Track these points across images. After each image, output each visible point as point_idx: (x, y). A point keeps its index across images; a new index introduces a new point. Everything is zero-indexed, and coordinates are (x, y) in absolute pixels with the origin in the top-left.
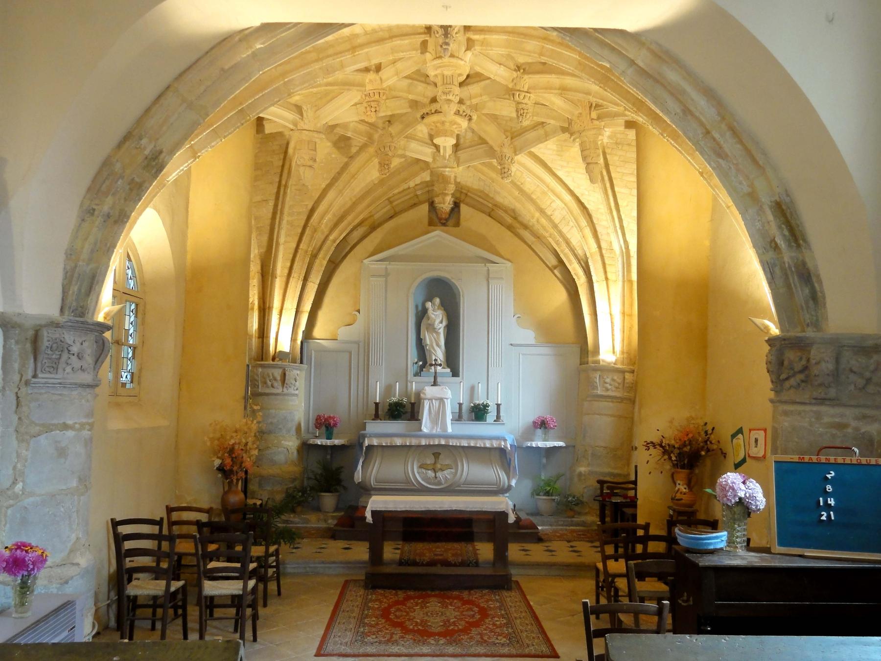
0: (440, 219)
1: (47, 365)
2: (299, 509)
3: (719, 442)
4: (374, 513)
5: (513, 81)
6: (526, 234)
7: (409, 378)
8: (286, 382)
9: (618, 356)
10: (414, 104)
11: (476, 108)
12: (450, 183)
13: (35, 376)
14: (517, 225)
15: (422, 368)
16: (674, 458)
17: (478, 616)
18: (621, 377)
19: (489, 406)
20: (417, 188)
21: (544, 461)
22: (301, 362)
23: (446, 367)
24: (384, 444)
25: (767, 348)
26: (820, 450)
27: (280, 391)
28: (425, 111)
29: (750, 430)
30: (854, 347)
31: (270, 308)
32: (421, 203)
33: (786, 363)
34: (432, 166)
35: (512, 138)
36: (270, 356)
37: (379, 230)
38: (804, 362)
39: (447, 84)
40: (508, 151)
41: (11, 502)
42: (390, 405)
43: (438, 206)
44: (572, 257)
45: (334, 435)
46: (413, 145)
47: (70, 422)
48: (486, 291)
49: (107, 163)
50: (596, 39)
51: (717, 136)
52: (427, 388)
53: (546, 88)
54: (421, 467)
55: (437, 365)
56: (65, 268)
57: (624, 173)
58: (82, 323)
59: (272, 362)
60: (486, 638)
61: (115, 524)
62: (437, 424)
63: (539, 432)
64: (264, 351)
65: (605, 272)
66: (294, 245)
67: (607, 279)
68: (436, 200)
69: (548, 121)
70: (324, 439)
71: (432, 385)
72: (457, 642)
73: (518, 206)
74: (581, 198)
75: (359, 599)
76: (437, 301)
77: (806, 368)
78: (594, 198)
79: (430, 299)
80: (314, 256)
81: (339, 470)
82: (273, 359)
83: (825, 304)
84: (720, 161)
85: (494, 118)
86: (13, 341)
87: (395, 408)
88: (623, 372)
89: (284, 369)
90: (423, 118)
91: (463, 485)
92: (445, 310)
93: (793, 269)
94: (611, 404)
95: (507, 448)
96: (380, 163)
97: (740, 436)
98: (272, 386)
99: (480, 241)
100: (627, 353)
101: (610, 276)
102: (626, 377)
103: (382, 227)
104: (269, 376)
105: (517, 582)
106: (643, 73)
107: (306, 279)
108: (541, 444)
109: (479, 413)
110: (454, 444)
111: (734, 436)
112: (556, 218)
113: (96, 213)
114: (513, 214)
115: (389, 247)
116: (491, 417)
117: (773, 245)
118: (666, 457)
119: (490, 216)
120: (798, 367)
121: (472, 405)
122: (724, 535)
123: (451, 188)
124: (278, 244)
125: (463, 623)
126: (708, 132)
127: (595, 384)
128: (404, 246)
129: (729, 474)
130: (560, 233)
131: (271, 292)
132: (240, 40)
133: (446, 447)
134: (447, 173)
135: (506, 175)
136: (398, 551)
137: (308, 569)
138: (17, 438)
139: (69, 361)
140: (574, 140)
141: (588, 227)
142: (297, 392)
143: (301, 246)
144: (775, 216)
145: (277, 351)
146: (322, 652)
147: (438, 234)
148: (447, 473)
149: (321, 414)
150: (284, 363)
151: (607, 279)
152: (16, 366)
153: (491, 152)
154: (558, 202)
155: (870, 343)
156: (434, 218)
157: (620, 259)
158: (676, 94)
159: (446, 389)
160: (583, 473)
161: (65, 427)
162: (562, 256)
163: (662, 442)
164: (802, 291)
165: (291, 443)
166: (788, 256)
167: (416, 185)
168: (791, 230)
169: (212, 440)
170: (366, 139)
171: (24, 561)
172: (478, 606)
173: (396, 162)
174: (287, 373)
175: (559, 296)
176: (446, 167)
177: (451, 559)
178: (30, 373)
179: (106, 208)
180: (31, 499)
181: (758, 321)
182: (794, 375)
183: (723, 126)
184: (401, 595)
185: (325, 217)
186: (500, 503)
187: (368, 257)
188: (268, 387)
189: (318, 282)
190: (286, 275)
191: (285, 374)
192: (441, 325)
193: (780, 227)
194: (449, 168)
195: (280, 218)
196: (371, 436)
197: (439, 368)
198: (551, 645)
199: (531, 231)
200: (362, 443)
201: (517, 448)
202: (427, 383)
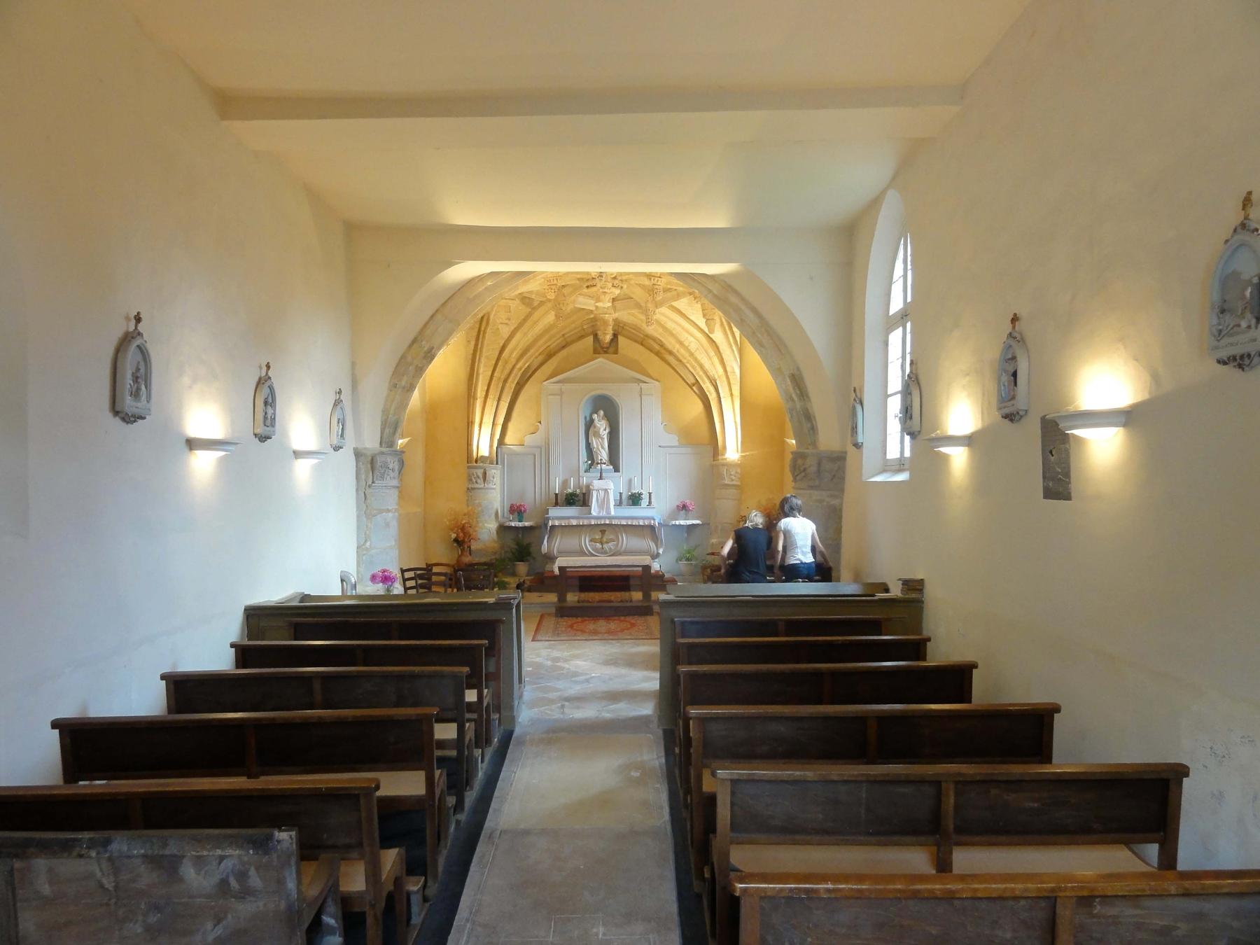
0: (602, 348)
4: (561, 568)
6: (671, 359)
7: (581, 474)
13: (373, 483)
14: (663, 351)
15: (591, 466)
17: (629, 626)
22: (497, 464)
27: (482, 486)
40: (650, 306)
41: (365, 552)
42: (567, 495)
45: (524, 520)
46: (581, 299)
47: (390, 508)
49: (403, 357)
58: (393, 451)
62: (603, 509)
66: (490, 373)
76: (602, 413)
77: (805, 470)
80: (505, 381)
81: (529, 545)
82: (476, 462)
90: (588, 287)
96: (556, 316)
98: (476, 482)
104: (474, 475)
106: (715, 296)
108: (682, 522)
109: (635, 499)
116: (645, 502)
119: (642, 344)
120: (802, 469)
124: (478, 374)
126: (754, 333)
130: (696, 360)
131: (473, 409)
133: (610, 525)
140: (697, 302)
143: (495, 375)
144: (791, 381)
145: (479, 455)
147: (601, 361)
152: (363, 477)
153: (638, 306)
156: (597, 345)
161: (388, 511)
165: (492, 526)
166: (798, 405)
168: (801, 393)
171: (390, 577)
175: (699, 407)
176: (606, 314)
179: (403, 383)
181: (788, 440)
184: (580, 619)
185: (512, 352)
197: (604, 466)
202: (594, 478)
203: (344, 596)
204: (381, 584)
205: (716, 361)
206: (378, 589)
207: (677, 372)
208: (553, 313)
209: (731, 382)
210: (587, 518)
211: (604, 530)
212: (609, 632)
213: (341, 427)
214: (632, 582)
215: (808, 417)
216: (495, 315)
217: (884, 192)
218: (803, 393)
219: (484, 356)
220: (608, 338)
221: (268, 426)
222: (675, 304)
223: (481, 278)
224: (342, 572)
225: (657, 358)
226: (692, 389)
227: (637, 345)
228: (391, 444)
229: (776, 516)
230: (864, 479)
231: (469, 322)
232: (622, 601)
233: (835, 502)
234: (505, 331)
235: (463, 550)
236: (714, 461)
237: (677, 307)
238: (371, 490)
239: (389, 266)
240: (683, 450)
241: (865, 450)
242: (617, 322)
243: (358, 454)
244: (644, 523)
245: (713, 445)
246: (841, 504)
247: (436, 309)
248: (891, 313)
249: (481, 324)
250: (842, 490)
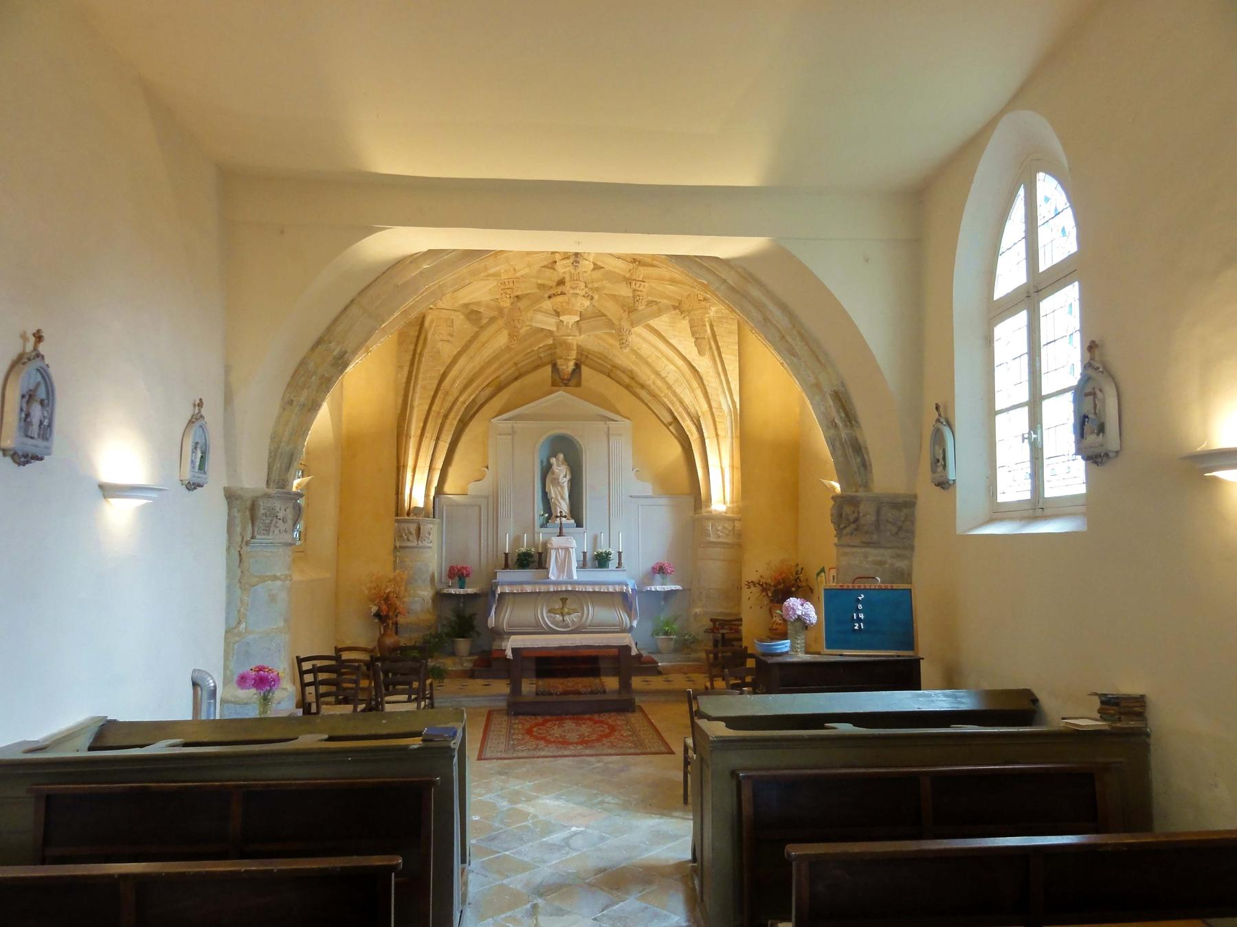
0: (562, 380)
1: (262, 528)
3: (807, 580)
4: (514, 650)
5: (630, 270)
6: (643, 393)
7: (536, 529)
8: (421, 535)
9: (728, 505)
10: (542, 287)
11: (597, 289)
12: (573, 350)
13: (253, 537)
14: (634, 384)
15: (549, 518)
16: (770, 595)
17: (607, 731)
21: (663, 603)
22: (434, 517)
24: (515, 591)
25: (832, 503)
26: (855, 580)
27: (415, 544)
28: (552, 292)
29: (830, 569)
30: (890, 503)
31: (405, 466)
33: (844, 515)
34: (556, 334)
35: (629, 312)
38: (856, 515)
39: (574, 280)
40: (625, 325)
42: (519, 555)
43: (561, 368)
44: (685, 415)
46: (539, 316)
47: (278, 574)
49: (303, 363)
50: (696, 262)
51: (789, 339)
52: (553, 538)
53: (659, 279)
55: (563, 517)
56: (270, 450)
57: (729, 342)
58: (284, 493)
59: (407, 517)
60: (615, 744)
61: (300, 661)
63: (658, 577)
65: (716, 429)
66: (426, 407)
67: (717, 435)
68: (559, 362)
69: (662, 301)
72: (592, 747)
73: (635, 368)
75: (503, 730)
76: (561, 456)
77: (857, 520)
78: (704, 364)
79: (555, 456)
80: (446, 416)
81: (472, 617)
82: (408, 514)
83: (871, 469)
84: (793, 358)
85: (614, 297)
86: (235, 510)
88: (732, 520)
90: (550, 297)
93: (848, 443)
95: (629, 591)
96: (509, 334)
97: (823, 574)
98: (408, 540)
99: (602, 401)
101: (720, 432)
102: (736, 525)
103: (508, 388)
105: (640, 706)
106: (732, 289)
108: (659, 588)
109: (602, 560)
111: (818, 574)
112: (671, 379)
113: (294, 403)
114: (630, 374)
115: (516, 407)
116: (613, 563)
117: (834, 424)
118: (764, 594)
120: (852, 518)
121: (595, 553)
122: (788, 642)
123: (573, 355)
124: (412, 407)
125: (595, 735)
126: (783, 337)
127: (708, 532)
128: (525, 407)
129: (791, 598)
130: (675, 393)
132: (411, 262)
133: (573, 592)
134: (570, 341)
135: (624, 345)
136: (534, 686)
137: (454, 703)
138: (240, 587)
139: (278, 525)
140: (684, 317)
142: (430, 545)
143: (433, 408)
146: (483, 757)
147: (561, 395)
148: (574, 617)
149: (454, 564)
150: (418, 518)
151: (717, 435)
152: (239, 529)
153: (610, 324)
154: (672, 367)
155: (900, 500)
157: (728, 417)
158: (759, 307)
160: (698, 613)
161: (275, 578)
162: (676, 414)
163: (759, 581)
164: (855, 460)
165: (426, 593)
166: (844, 433)
168: (847, 415)
169: (370, 589)
170: (496, 313)
171: (267, 679)
172: (607, 724)
173: (523, 331)
175: (676, 450)
176: (569, 336)
177: (583, 690)
178: (248, 537)
179: (302, 399)
180: (252, 637)
181: (826, 482)
182: (849, 525)
183: (794, 332)
184: (540, 719)
186: (625, 638)
187: (496, 416)
188: (404, 541)
191: (419, 528)
192: (565, 479)
193: (838, 411)
194: (572, 336)
195: (415, 383)
196: (503, 584)
197: (564, 519)
198: (669, 746)
199: (647, 389)
201: (638, 592)
203: (700, 387)
204: (253, 691)
205: (699, 393)
206: (247, 704)
207: (649, 408)
208: (505, 332)
209: (717, 420)
210: (545, 583)
211: (566, 598)
212: (584, 742)
213: (199, 455)
214: (603, 665)
215: (858, 448)
216: (433, 335)
217: (989, 126)
218: (850, 418)
219: (419, 386)
220: (571, 365)
221: (32, 438)
222: (653, 323)
223: (415, 259)
224: (194, 671)
225: (627, 392)
227: (603, 377)
228: (283, 484)
229: (793, 582)
230: (960, 530)
231: (395, 320)
232: (592, 693)
233: (902, 564)
234: (448, 351)
235: (386, 628)
236: (695, 514)
237: (655, 327)
238: (249, 549)
239: (282, 232)
240: (663, 501)
241: (961, 492)
242: (581, 350)
243: (231, 497)
245: (695, 496)
246: (911, 567)
247: (350, 298)
248: (997, 295)
249: (416, 345)
250: (912, 548)
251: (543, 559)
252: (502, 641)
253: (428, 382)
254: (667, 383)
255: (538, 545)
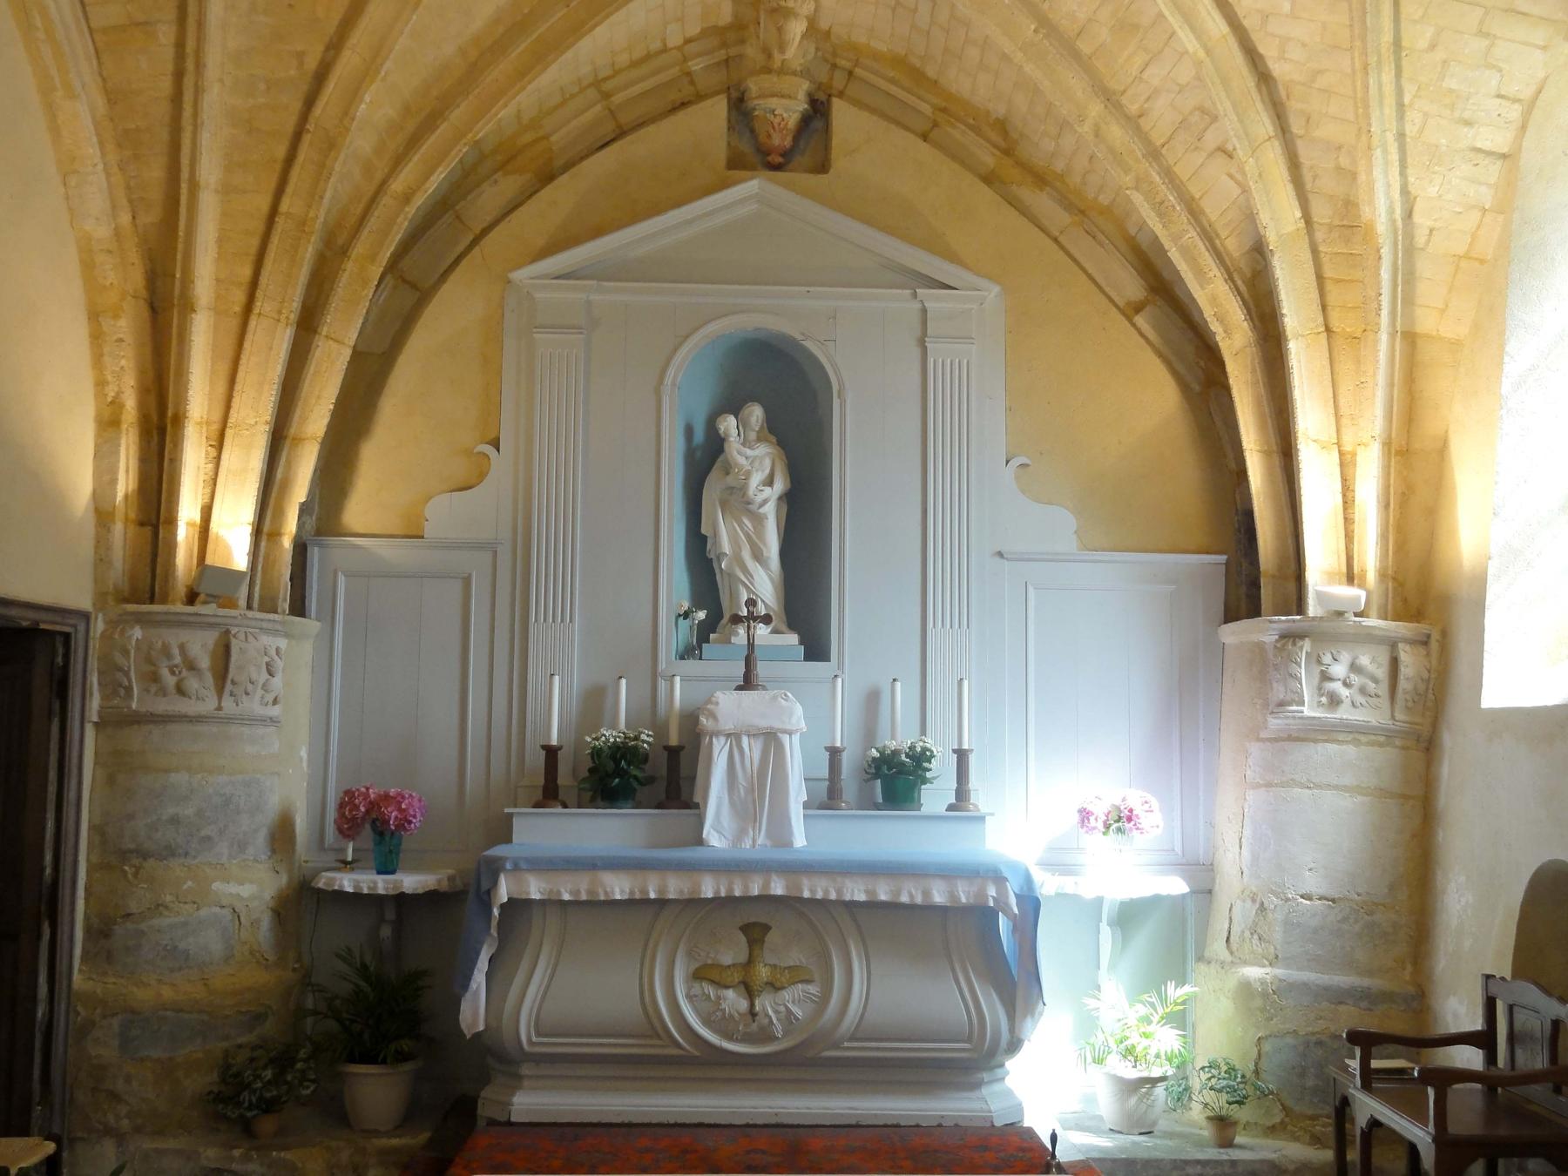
2: (267, 1125)
7: (662, 666)
8: (230, 676)
15: (705, 632)
18: (1384, 657)
19: (932, 756)
20: (692, 48)
22: (299, 607)
23: (784, 627)
24: (566, 897)
27: (208, 705)
31: (179, 420)
32: (700, 97)
36: (1122, 1149)
37: (563, 179)
42: (596, 753)
43: (761, 105)
44: (1207, 260)
48: (917, 366)
54: (698, 975)
55: (755, 619)
62: (755, 819)
64: (158, 571)
66: (263, 203)
70: (364, 869)
71: (739, 688)
74: (1257, 38)
76: (756, 413)
79: (732, 404)
83: (1376, 571)
87: (611, 766)
89: (227, 632)
91: (852, 1038)
92: (781, 443)
94: (1350, 750)
98: (180, 691)
100: (1394, 579)
104: (169, 656)
107: (308, 325)
110: (819, 895)
115: (598, 232)
116: (936, 795)
121: (875, 753)
124: (194, 186)
130: (1169, 175)
133: (790, 903)
141: (1276, 143)
142: (275, 711)
143: (284, 206)
156: (745, 147)
159: (786, 699)
167: (688, 41)
174: (235, 646)
188: (163, 692)
189: (352, 337)
190: (237, 309)
191: (227, 649)
192: (768, 490)
197: (762, 631)
200: (488, 892)
202: (721, 682)
207: (1062, 248)
226: (1134, 325)
244: (953, 896)
251: (684, 772)
252: (514, 1089)
253: (262, 100)
254: (1144, 138)
255: (666, 725)
